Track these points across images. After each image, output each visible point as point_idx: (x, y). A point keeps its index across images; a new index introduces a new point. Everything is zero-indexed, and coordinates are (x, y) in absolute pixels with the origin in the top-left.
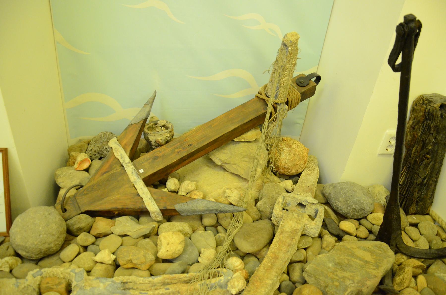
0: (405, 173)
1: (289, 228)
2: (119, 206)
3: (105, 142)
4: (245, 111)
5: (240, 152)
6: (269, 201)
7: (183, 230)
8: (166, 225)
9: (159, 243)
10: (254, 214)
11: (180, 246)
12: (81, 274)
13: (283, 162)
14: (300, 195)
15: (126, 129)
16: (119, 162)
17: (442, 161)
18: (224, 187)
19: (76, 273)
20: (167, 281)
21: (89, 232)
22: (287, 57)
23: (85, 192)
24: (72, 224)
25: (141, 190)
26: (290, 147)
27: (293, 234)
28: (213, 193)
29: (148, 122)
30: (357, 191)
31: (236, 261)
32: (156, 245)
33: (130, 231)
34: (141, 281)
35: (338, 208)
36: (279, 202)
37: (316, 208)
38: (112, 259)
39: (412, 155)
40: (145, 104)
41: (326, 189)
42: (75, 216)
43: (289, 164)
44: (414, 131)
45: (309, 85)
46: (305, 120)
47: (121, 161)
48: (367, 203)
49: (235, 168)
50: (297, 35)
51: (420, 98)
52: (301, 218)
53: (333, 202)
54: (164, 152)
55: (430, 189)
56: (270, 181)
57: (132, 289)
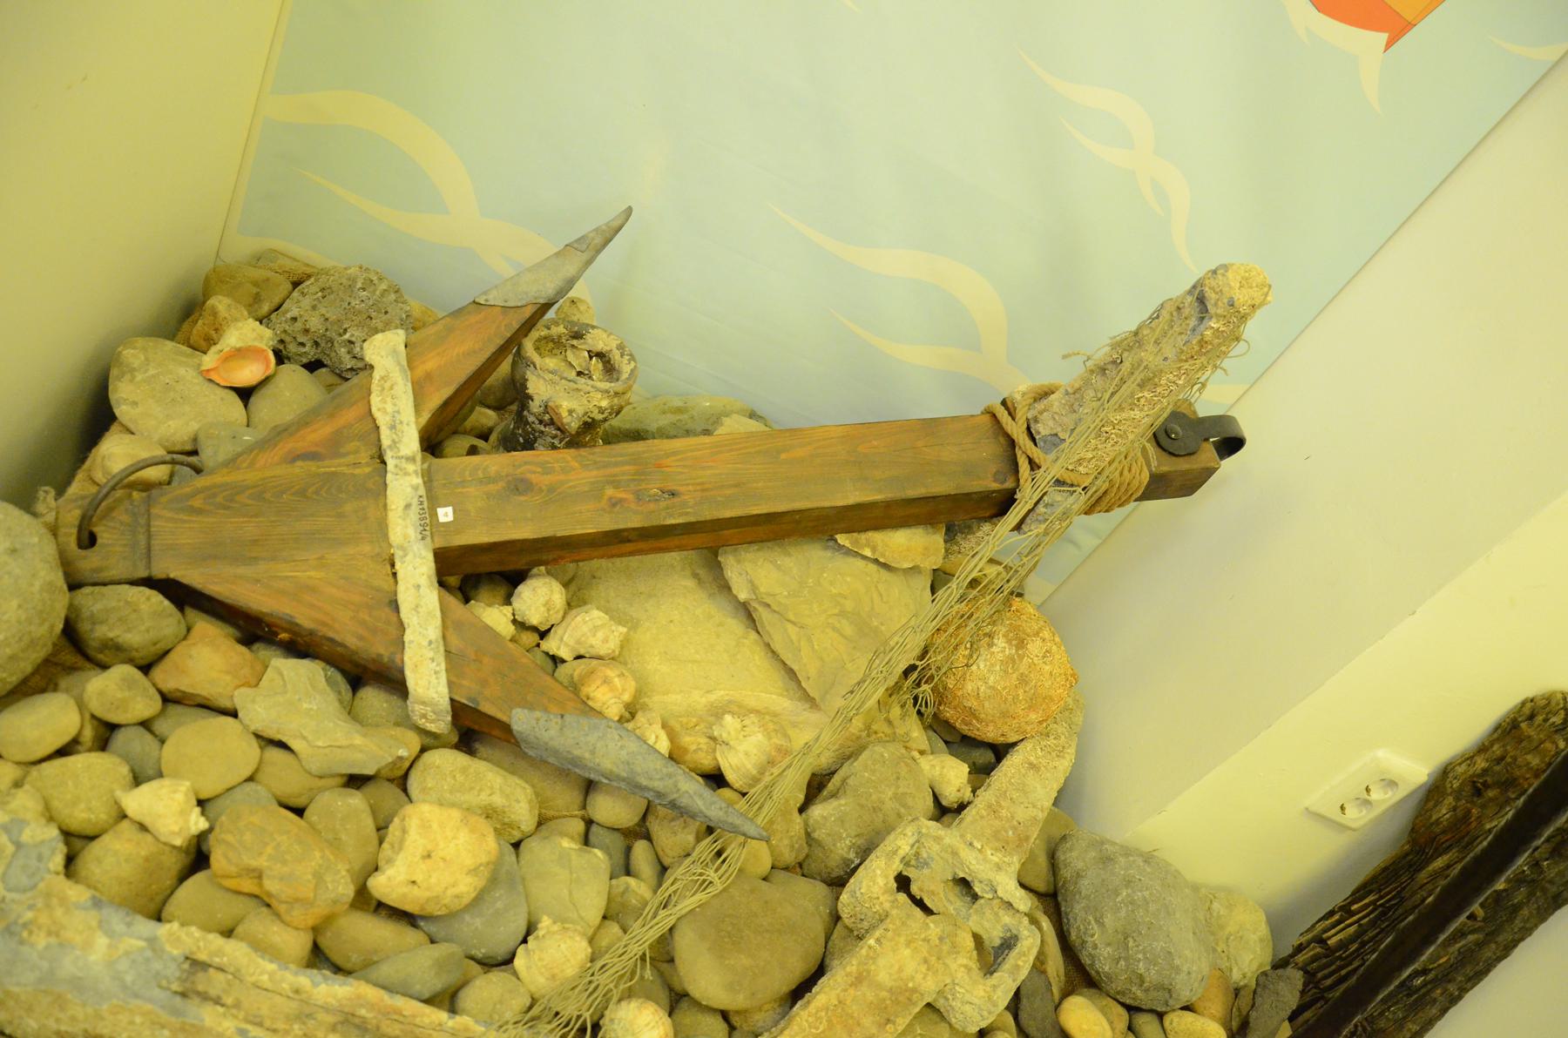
0: (1364, 917)
1: (890, 975)
2: (305, 618)
3: (357, 313)
4: (924, 449)
5: (834, 591)
6: (860, 817)
7: (506, 810)
8: (447, 760)
9: (397, 833)
10: (786, 842)
11: (470, 880)
12: (40, 858)
13: (969, 687)
14: (980, 851)
15: (458, 313)
16: (373, 436)
17: (1515, 946)
18: (722, 692)
19: (19, 845)
20: (363, 1012)
21: (146, 669)
22: (1185, 348)
23: (197, 503)
24: (92, 615)
25: (413, 590)
26: (1021, 644)
27: (897, 1002)
28: (672, 698)
29: (551, 314)
30: (1178, 916)
31: (652, 1024)
32: (381, 829)
33: (304, 738)
34: (265, 977)
35: (1084, 942)
36: (895, 852)
37: (1011, 927)
38: (189, 829)
39: (1423, 876)
40: (567, 243)
41: (1071, 850)
42: (119, 583)
43: (987, 704)
44: (1472, 802)
45: (1192, 457)
46: (1104, 541)
47: (386, 442)
48: (1189, 973)
49: (792, 641)
50: (1266, 289)
51: (1558, 704)
52: (949, 953)
53: (1078, 914)
54: (562, 477)
55: (1420, 1014)
56: (895, 733)
57: (217, 1001)
